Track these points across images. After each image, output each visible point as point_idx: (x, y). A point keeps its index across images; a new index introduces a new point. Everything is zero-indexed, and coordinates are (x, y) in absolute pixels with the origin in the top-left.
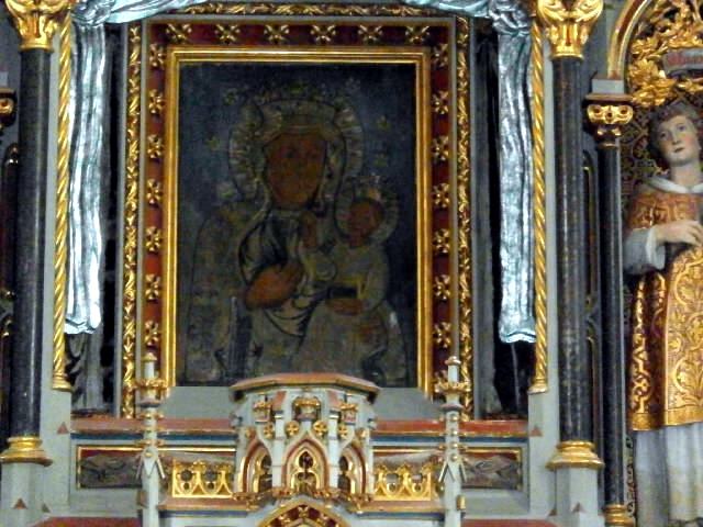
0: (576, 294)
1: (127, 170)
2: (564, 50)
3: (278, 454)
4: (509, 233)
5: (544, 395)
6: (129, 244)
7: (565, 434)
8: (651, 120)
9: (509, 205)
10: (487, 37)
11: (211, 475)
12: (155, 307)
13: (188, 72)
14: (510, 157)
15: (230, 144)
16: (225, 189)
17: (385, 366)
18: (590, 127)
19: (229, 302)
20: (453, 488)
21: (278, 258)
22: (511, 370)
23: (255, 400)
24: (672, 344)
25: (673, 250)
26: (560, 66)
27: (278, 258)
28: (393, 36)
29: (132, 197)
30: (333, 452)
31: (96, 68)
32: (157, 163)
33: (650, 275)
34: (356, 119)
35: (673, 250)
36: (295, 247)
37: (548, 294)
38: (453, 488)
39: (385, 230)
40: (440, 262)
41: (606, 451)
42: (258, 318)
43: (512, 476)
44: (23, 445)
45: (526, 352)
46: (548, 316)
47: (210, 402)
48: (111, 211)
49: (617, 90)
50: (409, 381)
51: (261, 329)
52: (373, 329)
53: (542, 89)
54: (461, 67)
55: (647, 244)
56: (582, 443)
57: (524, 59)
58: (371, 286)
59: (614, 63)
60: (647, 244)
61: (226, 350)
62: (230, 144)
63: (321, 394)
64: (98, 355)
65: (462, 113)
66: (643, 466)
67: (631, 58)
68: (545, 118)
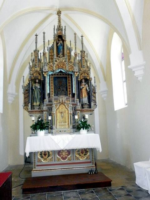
0: (77, 90)
1: (50, 83)
2: (76, 76)
3: (61, 100)
4: (73, 87)
5: (76, 96)
6: (51, 88)
7: (77, 98)
8: (82, 80)
9: (73, 85)
10: (71, 75)
11: (57, 102)
12: (52, 91)
13: (54, 77)
14: (73, 82)
15: (56, 82)
16: (56, 84)
17: (66, 95)
18: (78, 80)
19: (57, 91)
20: (71, 102)
21: (59, 88)
22: (73, 95)
23: (59, 97)
24: (83, 93)
25: (83, 87)
26: (76, 77)
27: (59, 88)
28: (66, 75)
29: (51, 85)
30: (64, 100)
31: (48, 77)
32: (52, 83)
33: (82, 89)
34: (64, 80)
35: (83, 87)
36: (61, 88)
37: (76, 90)
38: (71, 102)
39: (66, 87)
40: (69, 88)
41: (79, 99)
42: (58, 92)
43: (74, 101)
44: (45, 100)
45: (74, 94)
46: (76, 92)
47: (56, 97)
48: (49, 86)
49: (79, 78)
50: (67, 95)
51: (59, 93)
52: (65, 92)
53: (75, 78)
54: (70, 77)
55: (82, 87)
56: (40, 193)
57: (74, 76)
58: (65, 90)
59: (79, 77)
60: (82, 87)
61: (57, 94)
62: (56, 82)
63: (63, 97)
64: (49, 94)
65: (70, 79)
66: (81, 100)
67: (80, 76)
68: (75, 80)
